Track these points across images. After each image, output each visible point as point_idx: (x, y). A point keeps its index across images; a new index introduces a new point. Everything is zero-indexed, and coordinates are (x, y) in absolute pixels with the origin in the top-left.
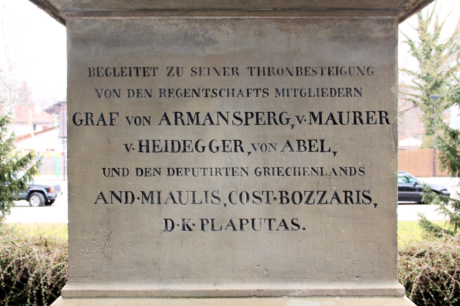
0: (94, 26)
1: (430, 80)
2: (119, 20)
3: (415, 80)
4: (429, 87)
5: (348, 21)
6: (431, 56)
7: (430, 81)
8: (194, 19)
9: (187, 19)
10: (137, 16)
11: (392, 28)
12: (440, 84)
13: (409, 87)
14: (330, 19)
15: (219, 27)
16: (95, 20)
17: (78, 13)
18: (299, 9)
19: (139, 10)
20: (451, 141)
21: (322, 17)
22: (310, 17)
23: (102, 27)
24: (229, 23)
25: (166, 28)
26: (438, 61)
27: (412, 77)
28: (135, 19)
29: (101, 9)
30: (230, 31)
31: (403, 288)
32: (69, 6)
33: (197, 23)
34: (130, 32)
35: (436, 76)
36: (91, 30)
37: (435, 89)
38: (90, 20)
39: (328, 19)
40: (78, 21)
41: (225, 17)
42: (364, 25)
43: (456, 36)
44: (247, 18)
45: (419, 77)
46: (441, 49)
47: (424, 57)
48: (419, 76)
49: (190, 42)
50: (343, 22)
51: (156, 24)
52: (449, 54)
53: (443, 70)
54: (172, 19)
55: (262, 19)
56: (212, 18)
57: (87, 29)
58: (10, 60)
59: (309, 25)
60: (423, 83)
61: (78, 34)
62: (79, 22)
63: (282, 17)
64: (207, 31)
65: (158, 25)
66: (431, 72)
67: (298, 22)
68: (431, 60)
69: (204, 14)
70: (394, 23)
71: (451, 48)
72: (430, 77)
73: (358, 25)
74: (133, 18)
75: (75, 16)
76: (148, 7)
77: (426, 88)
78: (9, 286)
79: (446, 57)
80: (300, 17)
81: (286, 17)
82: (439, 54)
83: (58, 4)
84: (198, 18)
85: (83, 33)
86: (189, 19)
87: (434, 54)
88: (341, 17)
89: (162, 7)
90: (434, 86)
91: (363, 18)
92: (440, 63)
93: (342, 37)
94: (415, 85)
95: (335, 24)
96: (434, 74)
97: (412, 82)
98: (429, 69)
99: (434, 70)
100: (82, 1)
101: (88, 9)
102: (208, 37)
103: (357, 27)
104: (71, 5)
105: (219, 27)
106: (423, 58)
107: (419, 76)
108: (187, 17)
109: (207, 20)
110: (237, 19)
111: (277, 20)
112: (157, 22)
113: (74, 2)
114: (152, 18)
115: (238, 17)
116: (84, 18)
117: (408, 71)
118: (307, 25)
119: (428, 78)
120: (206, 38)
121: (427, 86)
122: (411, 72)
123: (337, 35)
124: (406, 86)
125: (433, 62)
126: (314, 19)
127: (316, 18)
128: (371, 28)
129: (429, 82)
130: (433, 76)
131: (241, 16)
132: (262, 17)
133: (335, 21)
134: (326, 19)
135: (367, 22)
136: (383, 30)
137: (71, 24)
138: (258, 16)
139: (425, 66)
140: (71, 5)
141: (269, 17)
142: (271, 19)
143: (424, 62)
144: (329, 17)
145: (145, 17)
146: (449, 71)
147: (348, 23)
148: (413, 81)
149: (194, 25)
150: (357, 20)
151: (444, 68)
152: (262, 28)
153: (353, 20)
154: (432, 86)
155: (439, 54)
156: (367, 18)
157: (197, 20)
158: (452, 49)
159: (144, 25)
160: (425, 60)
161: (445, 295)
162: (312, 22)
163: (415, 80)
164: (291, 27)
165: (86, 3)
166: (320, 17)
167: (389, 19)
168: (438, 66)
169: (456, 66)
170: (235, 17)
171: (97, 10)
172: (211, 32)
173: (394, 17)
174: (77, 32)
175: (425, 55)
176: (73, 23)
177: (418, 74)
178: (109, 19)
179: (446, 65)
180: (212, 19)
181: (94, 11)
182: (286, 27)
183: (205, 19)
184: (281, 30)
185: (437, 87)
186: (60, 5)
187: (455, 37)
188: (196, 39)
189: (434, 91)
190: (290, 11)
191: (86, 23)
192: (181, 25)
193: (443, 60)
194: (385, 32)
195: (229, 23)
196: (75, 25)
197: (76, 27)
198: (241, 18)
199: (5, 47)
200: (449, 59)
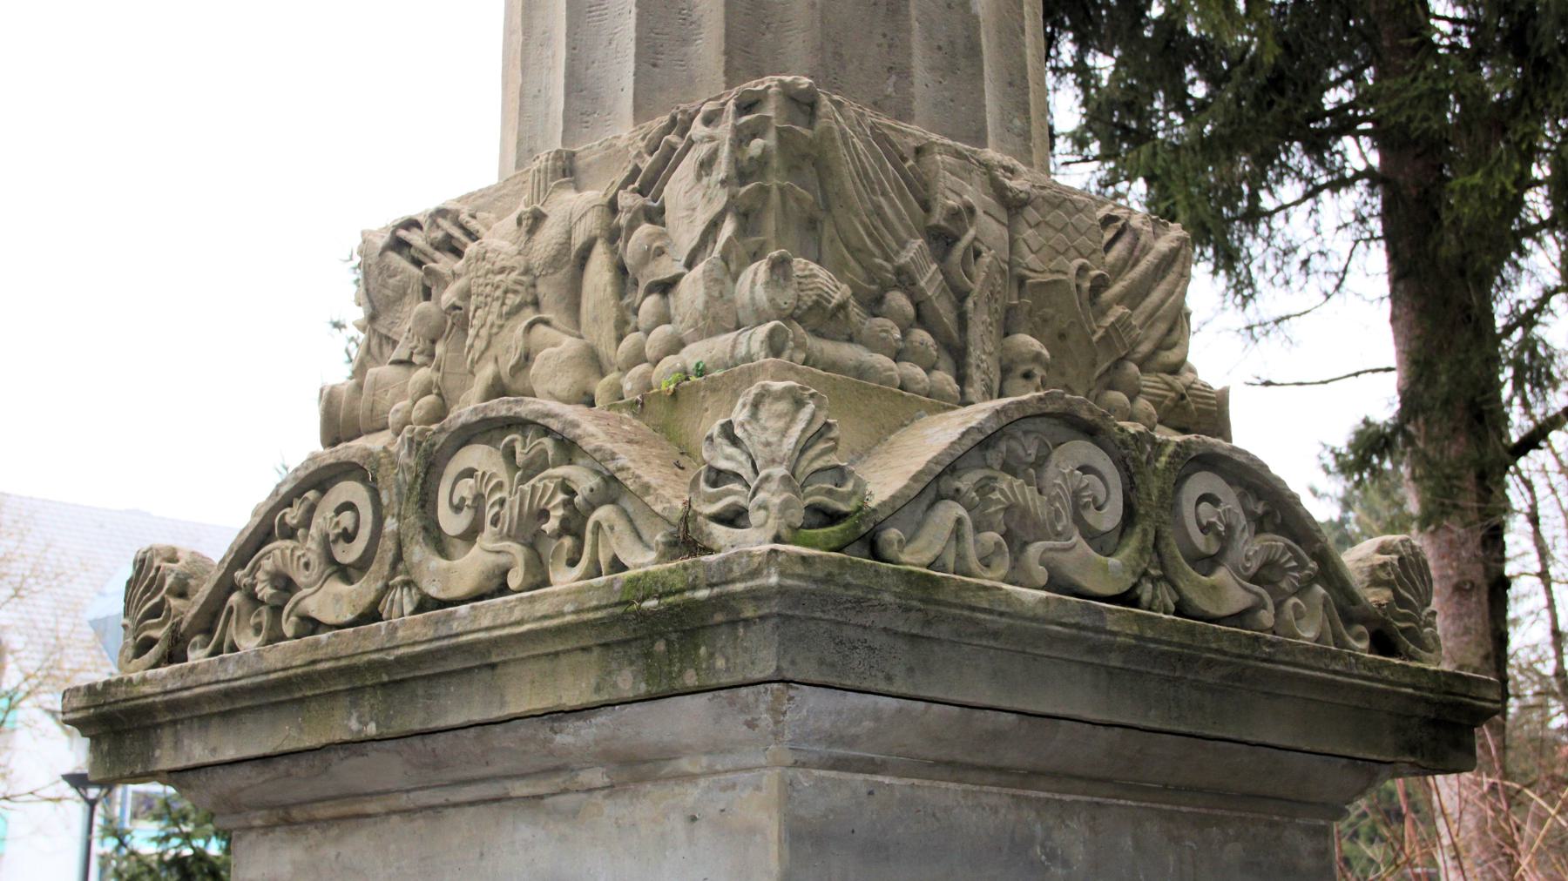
9: (1013, 796)
17: (821, 758)
20: (589, 165)
31: (951, 379)
36: (832, 811)
44: (1112, 805)
54: (987, 793)
74: (916, 781)
78: (1482, 505)
110: (1098, 803)
137: (789, 788)
161: (649, 198)
174: (802, 812)
196: (798, 791)
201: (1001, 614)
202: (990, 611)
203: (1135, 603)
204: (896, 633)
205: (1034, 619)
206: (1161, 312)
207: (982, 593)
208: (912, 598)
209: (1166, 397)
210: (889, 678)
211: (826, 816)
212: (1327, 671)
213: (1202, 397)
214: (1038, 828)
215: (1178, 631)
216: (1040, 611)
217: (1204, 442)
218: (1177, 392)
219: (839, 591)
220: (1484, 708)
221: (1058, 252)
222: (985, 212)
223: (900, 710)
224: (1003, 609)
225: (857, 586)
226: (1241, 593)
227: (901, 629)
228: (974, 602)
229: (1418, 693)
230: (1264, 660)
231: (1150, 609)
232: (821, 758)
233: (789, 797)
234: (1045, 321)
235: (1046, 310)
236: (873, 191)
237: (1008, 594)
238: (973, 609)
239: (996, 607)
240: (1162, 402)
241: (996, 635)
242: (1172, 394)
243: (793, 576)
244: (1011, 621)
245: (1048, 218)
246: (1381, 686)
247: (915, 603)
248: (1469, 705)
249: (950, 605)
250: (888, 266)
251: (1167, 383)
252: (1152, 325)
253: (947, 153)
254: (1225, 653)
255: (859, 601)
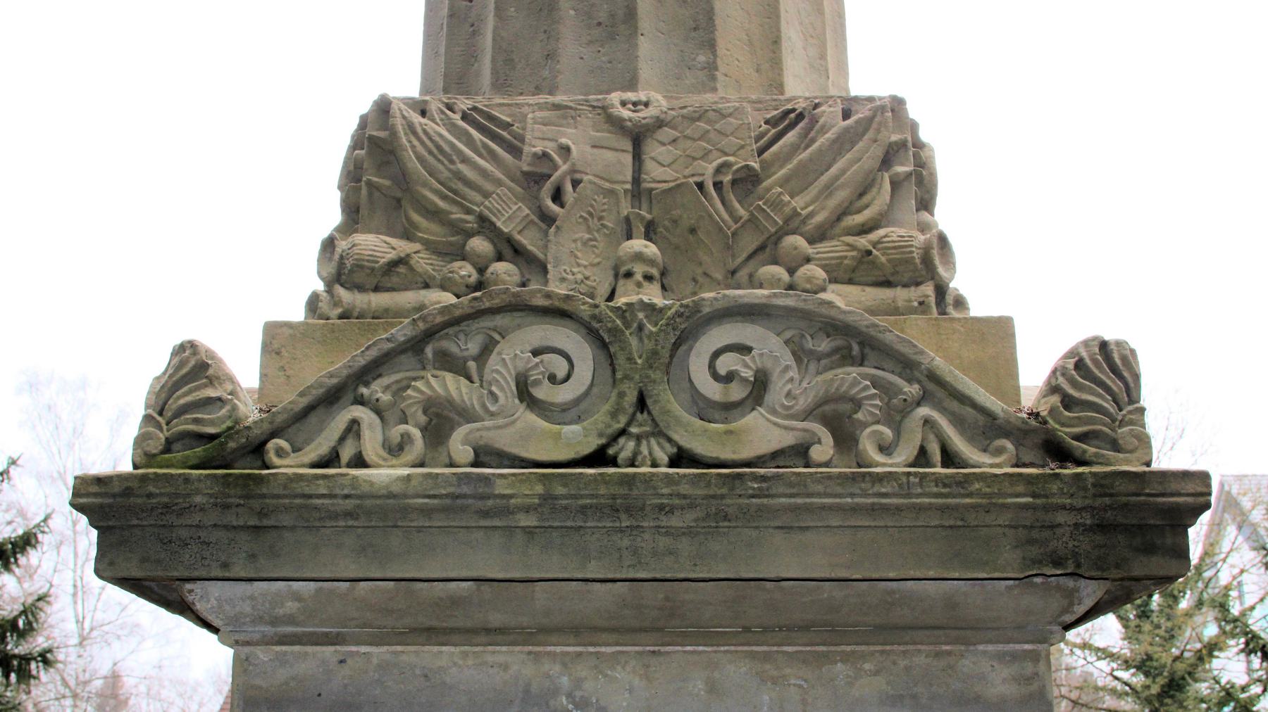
0: (302, 668)
1: (1156, 672)
2: (364, 653)
3: (1115, 673)
4: (1155, 690)
5: (926, 657)
6: (1152, 611)
7: (1158, 675)
8: (549, 653)
9: (530, 653)
10: (408, 645)
11: (1037, 674)
12: (1181, 682)
13: (1103, 689)
14: (882, 652)
15: (609, 672)
16: (306, 652)
17: (264, 636)
18: (805, 628)
19: (413, 630)
21: (863, 648)
22: (832, 648)
23: (321, 670)
24: (633, 663)
25: (479, 674)
26: (1169, 624)
27: (1109, 664)
28: (403, 652)
29: (322, 627)
30: (636, 681)
32: (243, 620)
33: (554, 663)
34: (390, 684)
35: (1169, 661)
36: (293, 679)
37: (1172, 697)
38: (292, 653)
39: (878, 651)
40: (261, 656)
41: (624, 649)
42: (967, 665)
43: (1208, 561)
44: (678, 651)
45: (1127, 664)
46: (1176, 593)
47: (1135, 613)
48: (1126, 662)
49: (536, 708)
50: (914, 659)
51: (455, 664)
52: (1197, 606)
53: (1185, 646)
55: (715, 652)
56: (591, 649)
57: (282, 674)
58: (84, 618)
59: (830, 666)
60: (1138, 680)
61: (261, 688)
62: (266, 659)
63: (765, 648)
64: (578, 683)
65: (460, 667)
66: (1156, 653)
67: (804, 660)
68: (1152, 622)
69: (572, 640)
70: (1039, 661)
71: (1200, 590)
72: (1155, 664)
73: (951, 667)
74: (399, 648)
75: (257, 644)
76: (435, 623)
77: (1147, 693)
79: (1188, 614)
80: (808, 648)
81: (775, 648)
82: (1170, 607)
83: (217, 617)
84: (558, 649)
85: (272, 686)
86: (535, 653)
87: (1159, 605)
88: (911, 647)
89: (469, 624)
90: (1166, 689)
91: (963, 648)
92: (1176, 628)
93: (914, 697)
94: (1119, 686)
95: (894, 663)
96: (1165, 658)
97: (1110, 678)
98: (1151, 644)
99: (1164, 646)
100: (276, 611)
101: (289, 629)
102: (582, 697)
103: (950, 671)
104: (248, 619)
105: (609, 672)
106: (1131, 616)
107: (1126, 662)
108: (530, 647)
109: (580, 654)
110: (654, 652)
111: (753, 656)
112: (456, 659)
113: (256, 613)
114: (444, 648)
115: (656, 648)
116: (278, 648)
117: (1098, 649)
118: (827, 667)
119: (1151, 667)
120: (577, 699)
121: (1148, 687)
122: (1103, 650)
123: (902, 692)
124: (1097, 689)
125: (1158, 627)
126: (843, 652)
127: (849, 648)
128: (983, 673)
129: (1154, 678)
130: (1163, 661)
131: (662, 645)
132: (715, 648)
133: (895, 657)
134: (872, 653)
135: (973, 660)
136: (1014, 679)
137: (246, 664)
138: (705, 645)
139: (1140, 637)
140: (248, 619)
141: (732, 648)
142: (737, 652)
143: (1136, 627)
144: (879, 648)
145: (427, 648)
146: (1200, 651)
147: (929, 660)
148: (1111, 674)
149: (547, 667)
150: (949, 653)
151: (1187, 643)
152: (716, 675)
153: (938, 655)
154: (1163, 686)
155: (1170, 607)
156: (972, 648)
157: (554, 654)
158: (1201, 593)
159: (424, 667)
160: (1138, 620)
162: (838, 658)
163: (1119, 674)
164: (788, 671)
165: (284, 616)
166: (858, 648)
167: (1025, 651)
168: (1173, 637)
169: (1217, 636)
170: (648, 648)
171: (311, 629)
172: (589, 686)
173: (1039, 645)
174: (258, 682)
175: (1136, 610)
176: (250, 659)
177: (1123, 658)
178: (340, 651)
179: (1191, 635)
180: (591, 653)
181: (303, 632)
182: (775, 673)
183: (575, 652)
184: (763, 681)
185: (1176, 691)
186: (222, 620)
187: (1207, 565)
188: (552, 703)
189: (1168, 701)
190: (784, 633)
191: (282, 660)
192: (515, 667)
193: (1182, 622)
194: (1020, 684)
195: (633, 663)
196: (256, 665)
197: (258, 671)
198: (663, 649)
199: (75, 586)
200: (1198, 619)
201: (347, 497)
202: (331, 496)
203: (613, 462)
204: (234, 527)
205: (391, 495)
206: (842, 180)
207: (321, 482)
208: (229, 496)
209: (846, 257)
210: (225, 566)
211: (286, 683)
212: (866, 495)
213: (895, 248)
214: (565, 680)
215: (606, 483)
216: (396, 489)
217: (725, 296)
218: (859, 250)
219: (139, 501)
220: (1178, 504)
221: (694, 159)
222: (594, 147)
223: (319, 590)
224: (346, 492)
225: (161, 494)
226: (777, 432)
227: (235, 523)
228: (307, 491)
229: (1038, 501)
230: (753, 496)
231: (632, 465)
232: (264, 636)
233: (245, 670)
234: (675, 222)
235: (674, 212)
236: (452, 162)
237: (355, 478)
238: (310, 497)
239: (338, 491)
240: (841, 263)
241: (348, 514)
242: (854, 253)
243: (88, 495)
244: (359, 502)
245: (688, 132)
246: (968, 500)
247: (232, 500)
248: (1145, 503)
249: (278, 497)
250: (469, 218)
251: (848, 245)
252: (830, 194)
253: (541, 109)
254: (685, 497)
255: (166, 506)
